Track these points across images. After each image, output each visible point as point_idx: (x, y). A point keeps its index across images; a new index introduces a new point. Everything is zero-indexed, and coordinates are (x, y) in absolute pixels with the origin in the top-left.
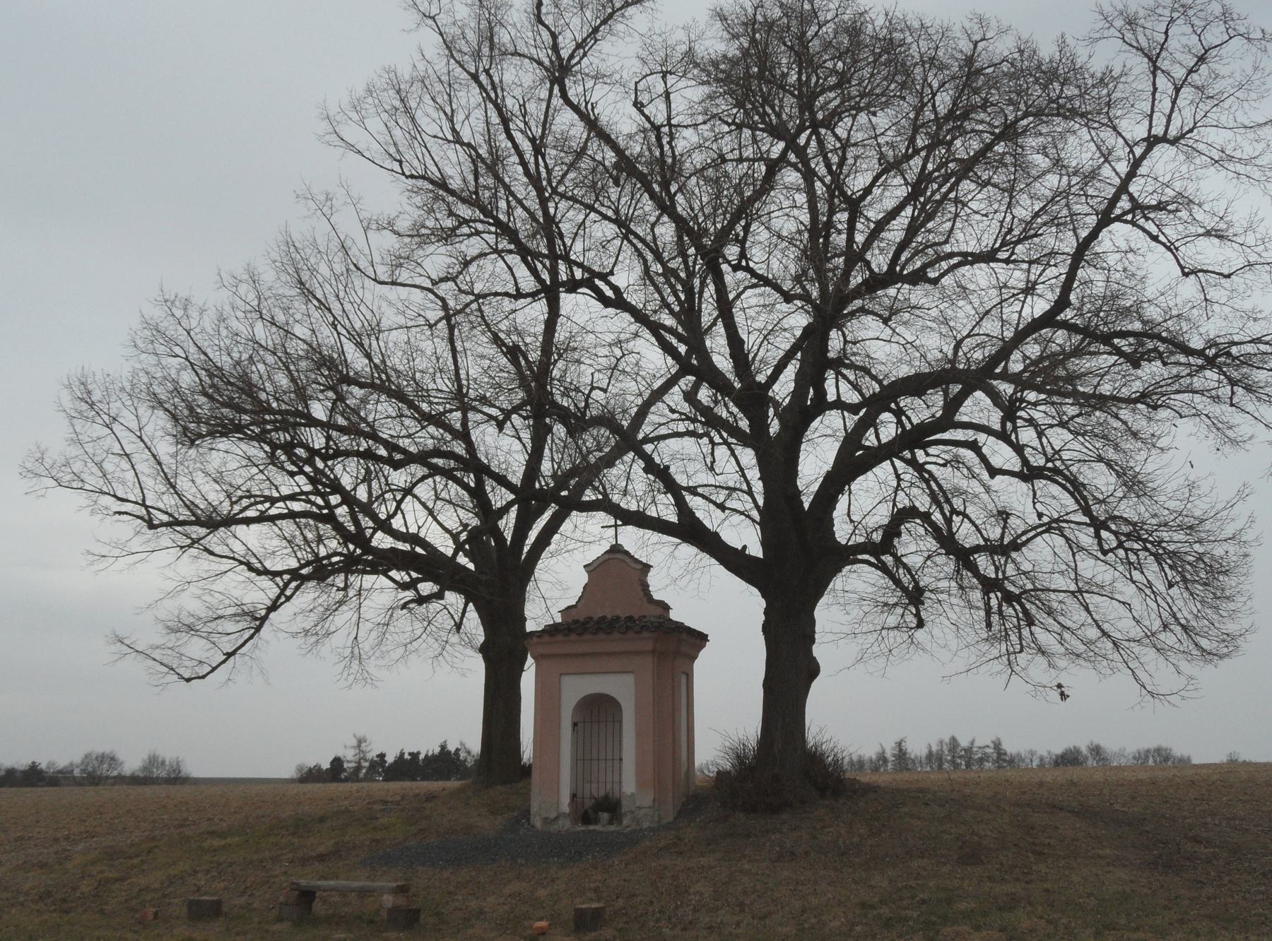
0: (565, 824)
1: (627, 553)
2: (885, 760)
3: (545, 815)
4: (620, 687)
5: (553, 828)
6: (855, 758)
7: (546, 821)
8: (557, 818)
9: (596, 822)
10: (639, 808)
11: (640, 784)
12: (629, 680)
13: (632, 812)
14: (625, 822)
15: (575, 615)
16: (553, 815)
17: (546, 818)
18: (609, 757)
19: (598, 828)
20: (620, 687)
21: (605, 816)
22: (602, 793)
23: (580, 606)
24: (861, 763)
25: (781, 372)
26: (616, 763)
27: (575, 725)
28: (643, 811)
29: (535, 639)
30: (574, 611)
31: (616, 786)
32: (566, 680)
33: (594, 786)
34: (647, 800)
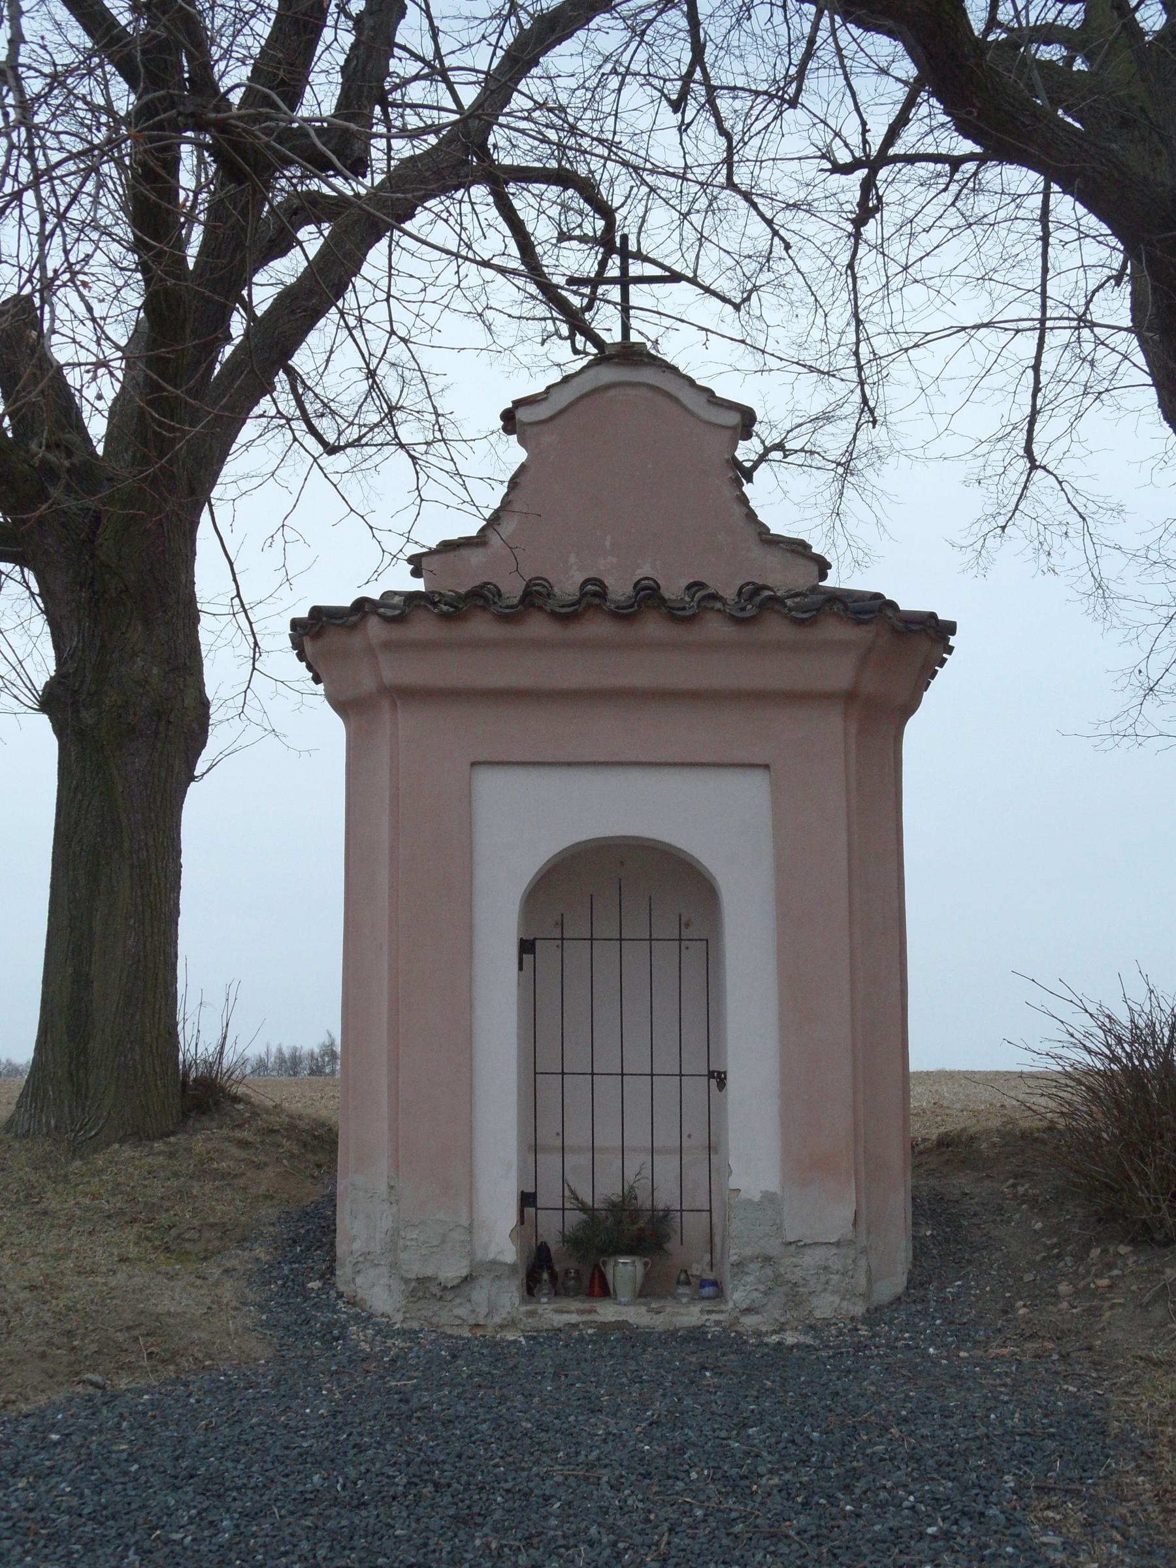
0: (501, 1304)
1: (673, 369)
2: (333, 1055)
3: (417, 1269)
4: (718, 818)
5: (455, 1317)
6: (287, 1053)
7: (422, 1289)
8: (467, 1280)
9: (601, 1289)
10: (799, 1246)
11: (803, 1164)
12: (751, 791)
13: (767, 1259)
14: (738, 1296)
15: (473, 571)
16: (451, 1271)
17: (422, 1281)
18: (666, 1062)
19: (607, 1312)
20: (718, 818)
21: (625, 1270)
22: (609, 1188)
23: (495, 541)
24: (291, 1064)
25: (719, 113)
26: (696, 1088)
27: (526, 947)
28: (811, 1259)
29: (374, 627)
30: (476, 557)
31: (696, 1174)
32: (493, 787)
33: (578, 1161)
34: (829, 1215)
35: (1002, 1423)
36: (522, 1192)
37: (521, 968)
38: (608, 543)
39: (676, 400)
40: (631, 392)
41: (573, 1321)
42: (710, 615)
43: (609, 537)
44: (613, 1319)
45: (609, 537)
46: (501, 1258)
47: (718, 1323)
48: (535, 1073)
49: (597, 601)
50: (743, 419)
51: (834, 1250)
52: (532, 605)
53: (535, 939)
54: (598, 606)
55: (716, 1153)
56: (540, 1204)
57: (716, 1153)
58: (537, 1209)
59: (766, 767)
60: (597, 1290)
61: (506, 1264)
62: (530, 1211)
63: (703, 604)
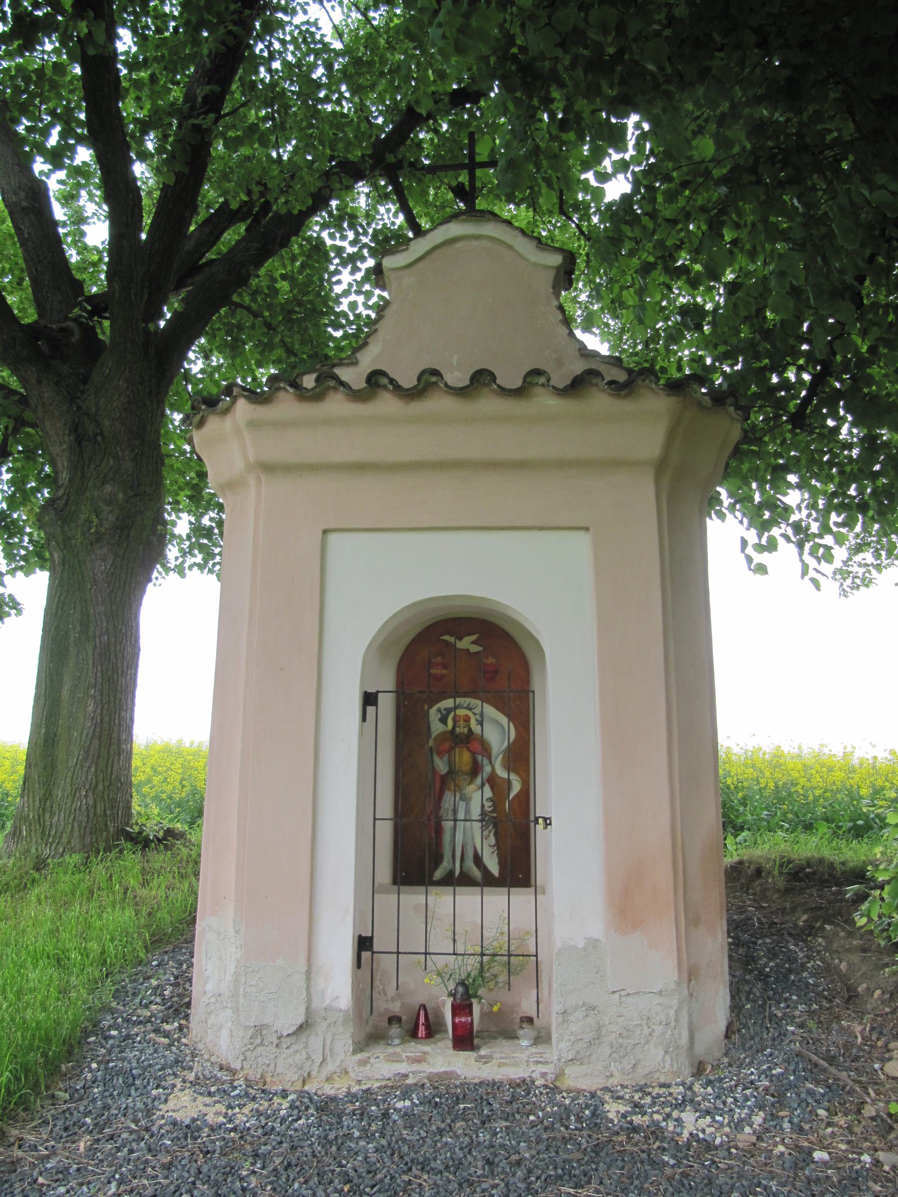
12: (577, 548)
14: (561, 1046)
35: (154, 1100)
36: (360, 936)
37: (364, 718)
38: (455, 361)
39: (511, 247)
40: (475, 243)
41: (403, 1071)
42: (539, 390)
43: (455, 357)
44: (442, 1070)
45: (455, 357)
46: (336, 1004)
47: (544, 1075)
48: (375, 819)
49: (434, 379)
50: (565, 259)
51: (659, 1000)
52: (378, 386)
53: (378, 692)
54: (435, 383)
55: (544, 893)
56: (375, 949)
57: (544, 893)
58: (373, 953)
59: (587, 529)
60: (422, 1031)
61: (340, 1010)
62: (366, 955)
63: (529, 380)
